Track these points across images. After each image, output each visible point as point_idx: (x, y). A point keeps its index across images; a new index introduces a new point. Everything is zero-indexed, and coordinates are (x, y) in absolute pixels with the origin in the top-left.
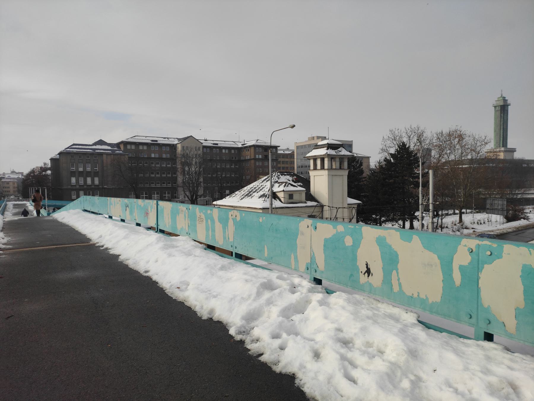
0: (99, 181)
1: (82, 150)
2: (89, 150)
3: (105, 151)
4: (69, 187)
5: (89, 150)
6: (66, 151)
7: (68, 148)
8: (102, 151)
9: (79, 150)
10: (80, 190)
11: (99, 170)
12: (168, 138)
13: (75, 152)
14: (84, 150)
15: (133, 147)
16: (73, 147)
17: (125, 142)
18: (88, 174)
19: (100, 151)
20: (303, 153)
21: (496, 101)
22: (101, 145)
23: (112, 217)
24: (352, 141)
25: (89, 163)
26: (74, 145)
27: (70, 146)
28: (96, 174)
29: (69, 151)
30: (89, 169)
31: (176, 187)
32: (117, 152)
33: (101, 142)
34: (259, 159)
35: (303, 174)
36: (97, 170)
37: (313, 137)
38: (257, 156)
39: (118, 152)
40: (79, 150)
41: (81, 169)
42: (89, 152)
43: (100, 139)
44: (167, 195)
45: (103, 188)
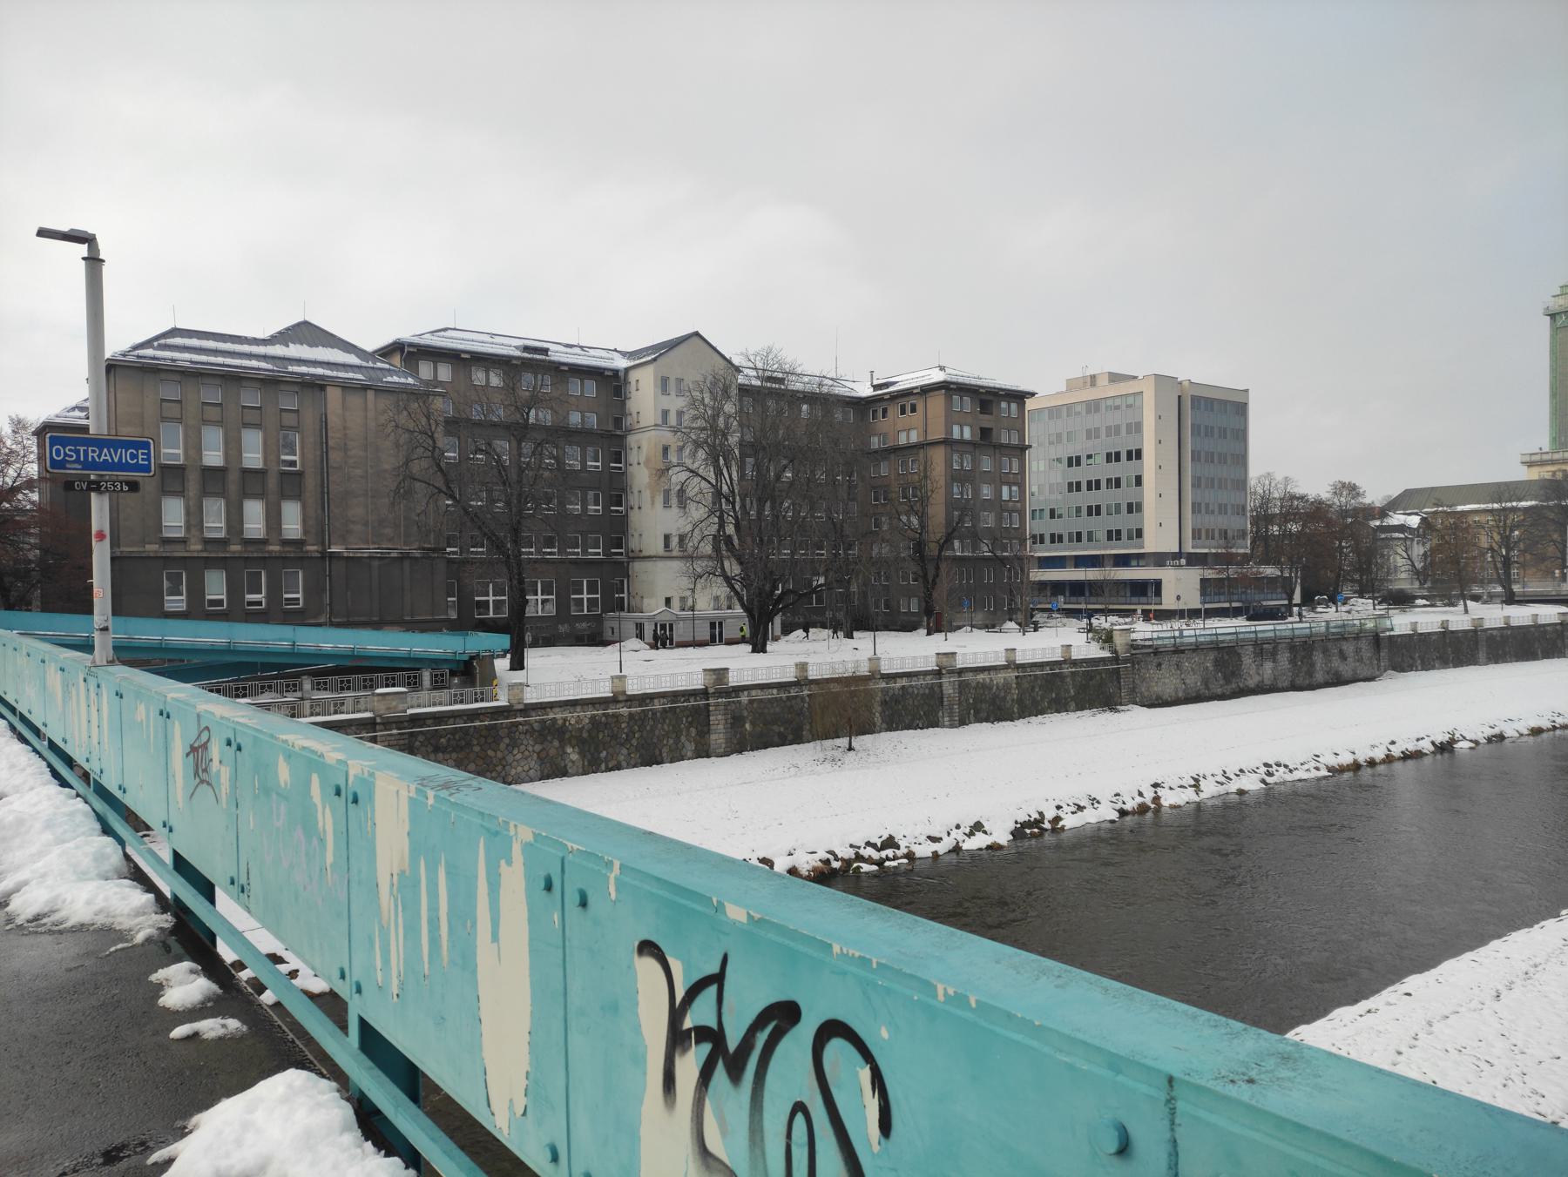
0: (304, 521)
1: (220, 360)
2: (254, 363)
3: (335, 374)
4: (148, 547)
5: (254, 363)
6: (138, 357)
7: (148, 344)
8: (320, 371)
9: (203, 358)
10: (210, 563)
11: (303, 464)
12: (582, 348)
13: (188, 364)
14: (229, 361)
15: (445, 373)
16: (162, 341)
17: (411, 345)
18: (252, 483)
19: (312, 370)
20: (1059, 436)
21: (1554, 296)
22: (312, 344)
23: (522, 668)
24: (1247, 391)
25: (258, 426)
26: (175, 332)
27: (157, 338)
28: (291, 484)
29: (154, 358)
30: (253, 457)
31: (623, 558)
32: (389, 379)
33: (305, 332)
34: (962, 442)
35: (1060, 516)
36: (293, 463)
37: (1093, 377)
38: (956, 435)
39: (395, 379)
40: (203, 358)
41: (213, 457)
42: (259, 369)
43: (300, 319)
44: (585, 596)
45: (325, 556)
